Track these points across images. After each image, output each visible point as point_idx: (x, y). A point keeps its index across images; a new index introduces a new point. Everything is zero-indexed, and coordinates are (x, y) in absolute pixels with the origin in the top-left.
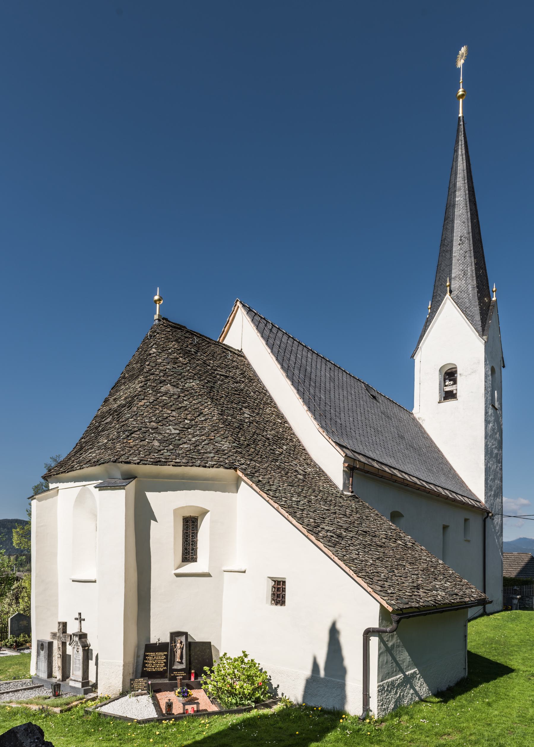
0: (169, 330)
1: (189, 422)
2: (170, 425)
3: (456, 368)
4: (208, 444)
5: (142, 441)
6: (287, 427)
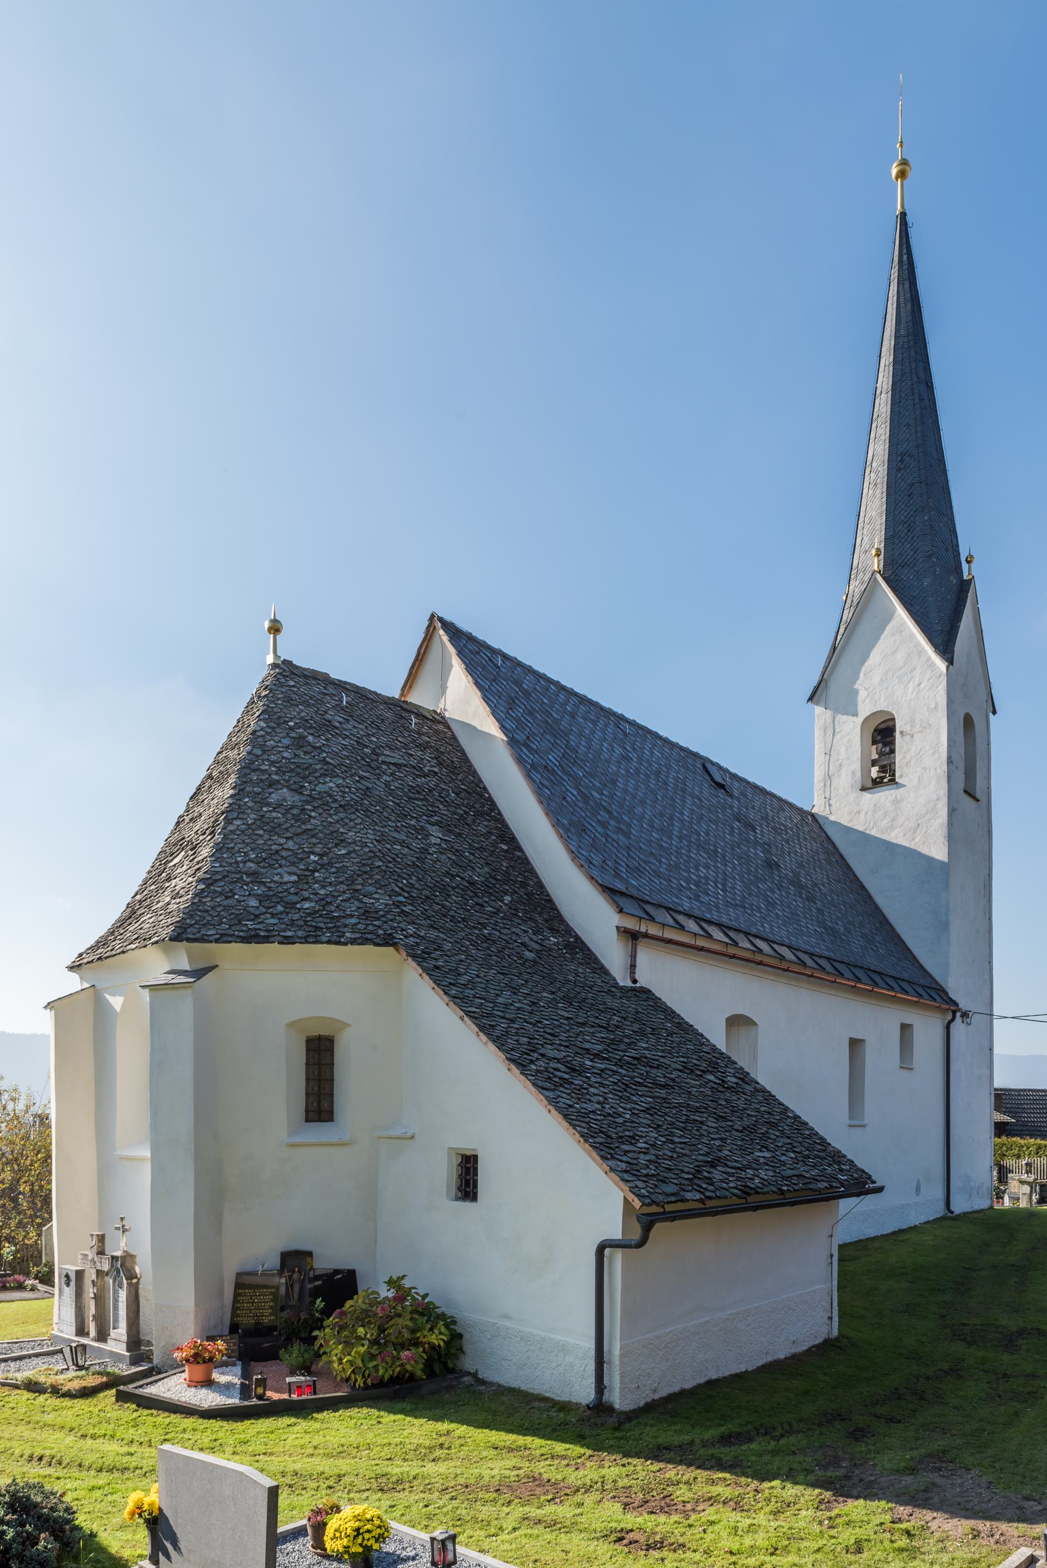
0: (293, 683)
1: (316, 859)
2: (281, 866)
3: (894, 719)
4: (349, 899)
5: (227, 898)
6: (519, 857)
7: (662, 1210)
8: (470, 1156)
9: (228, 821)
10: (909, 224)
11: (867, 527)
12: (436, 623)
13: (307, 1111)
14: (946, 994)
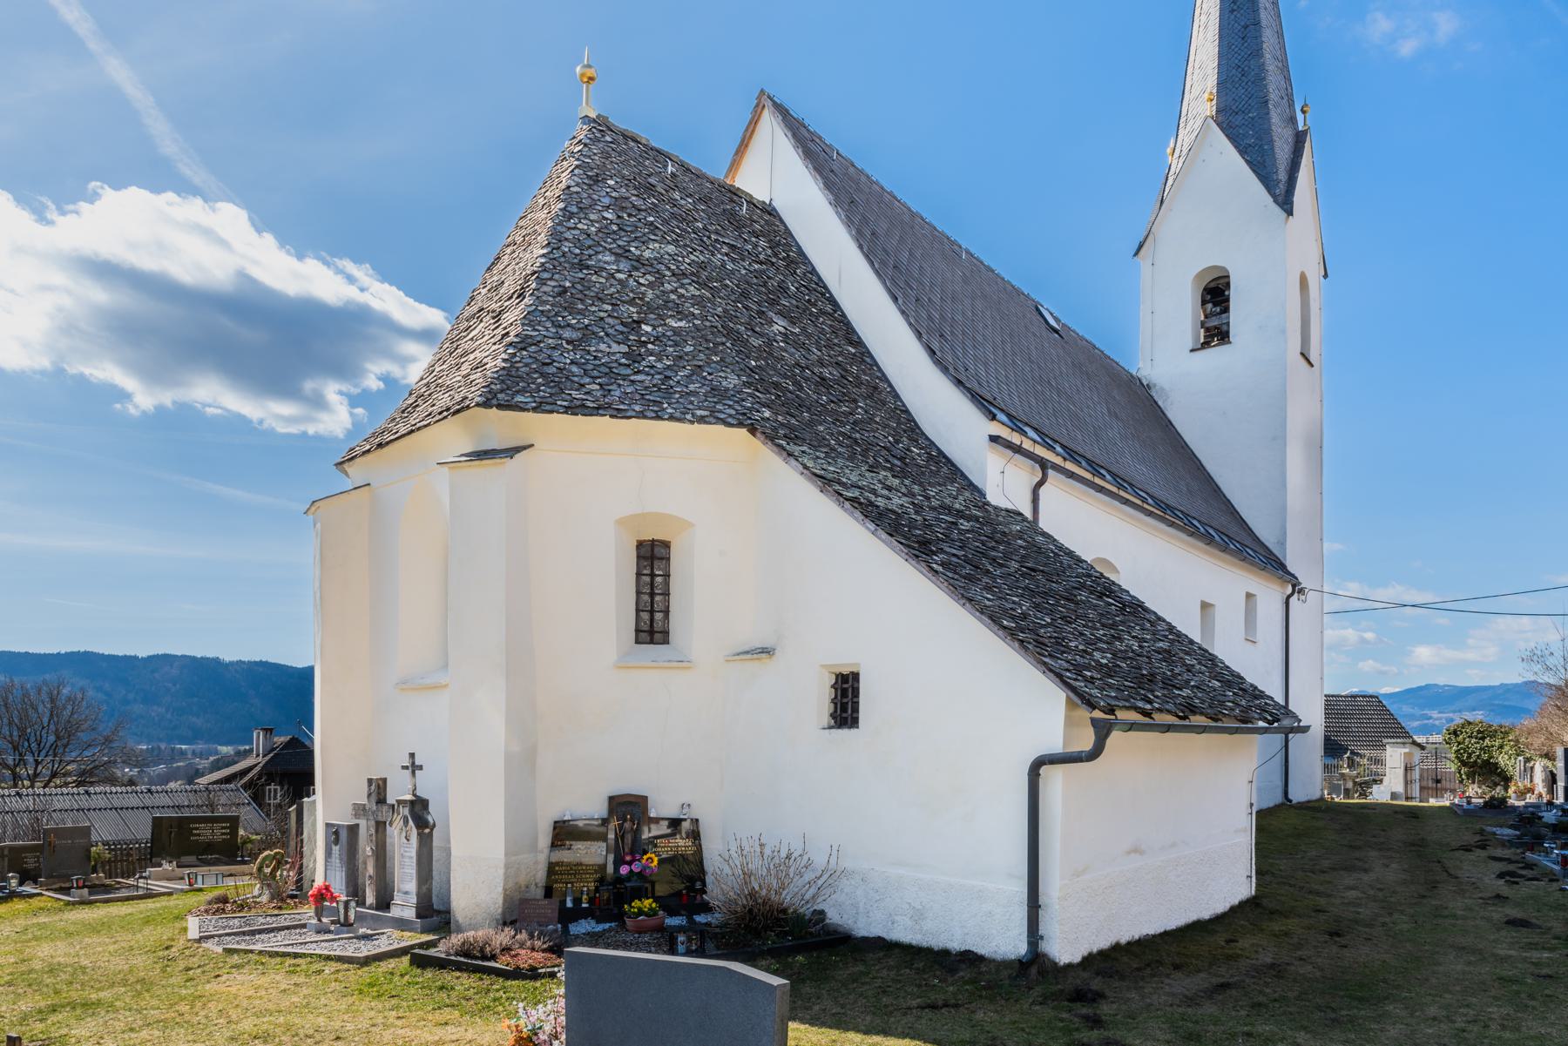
12: (766, 101)
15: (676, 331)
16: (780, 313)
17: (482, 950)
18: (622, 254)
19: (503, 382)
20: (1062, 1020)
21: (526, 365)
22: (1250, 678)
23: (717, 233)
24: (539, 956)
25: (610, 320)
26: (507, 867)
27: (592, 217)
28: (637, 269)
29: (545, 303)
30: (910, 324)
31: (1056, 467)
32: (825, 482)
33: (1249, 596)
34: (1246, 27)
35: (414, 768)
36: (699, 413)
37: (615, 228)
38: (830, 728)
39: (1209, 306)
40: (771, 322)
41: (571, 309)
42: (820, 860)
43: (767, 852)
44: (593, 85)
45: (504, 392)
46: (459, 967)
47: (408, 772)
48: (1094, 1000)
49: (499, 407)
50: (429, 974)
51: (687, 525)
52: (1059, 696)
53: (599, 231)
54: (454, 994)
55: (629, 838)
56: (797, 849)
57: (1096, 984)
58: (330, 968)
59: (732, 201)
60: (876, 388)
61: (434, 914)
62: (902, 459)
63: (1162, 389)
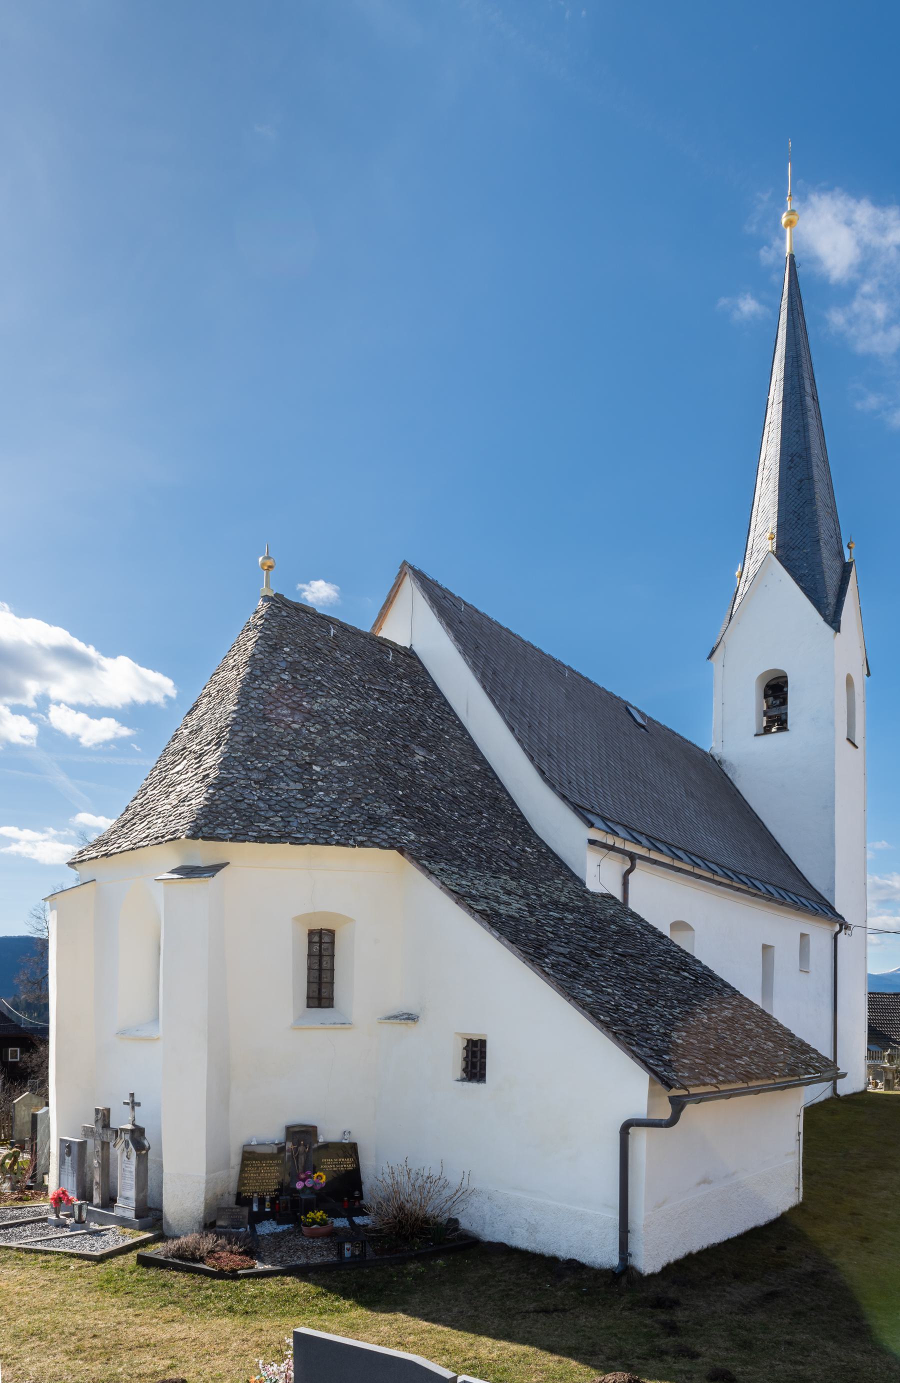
3: (786, 677)
7: (686, 1093)
8: (477, 1041)
9: (233, 733)
10: (797, 265)
11: (760, 514)
12: (407, 569)
13: (308, 998)
14: (834, 909)
15: (340, 770)
16: (422, 745)
17: (193, 1254)
18: (296, 708)
19: (206, 817)
20: (646, 1326)
21: (224, 802)
22: (799, 1033)
23: (370, 682)
24: (237, 1258)
25: (288, 763)
26: (207, 1182)
27: (273, 678)
28: (308, 720)
29: (237, 750)
30: (524, 750)
31: (642, 858)
32: (462, 897)
33: (803, 935)
34: (801, 481)
35: (134, 1104)
36: (359, 838)
37: (290, 686)
38: (463, 1080)
39: (771, 699)
40: (413, 754)
41: (259, 757)
42: (454, 1180)
43: (413, 1176)
44: (271, 572)
45: (207, 826)
46: (176, 1268)
47: (129, 1107)
48: (671, 1307)
49: (204, 838)
50: (152, 1272)
51: (348, 920)
52: (644, 1077)
53: (278, 689)
54: (174, 1291)
55: (302, 1159)
56: (436, 1173)
57: (672, 1293)
58: (74, 1264)
59: (381, 651)
60: (497, 799)
61: (150, 1214)
62: (517, 860)
63: (731, 764)
